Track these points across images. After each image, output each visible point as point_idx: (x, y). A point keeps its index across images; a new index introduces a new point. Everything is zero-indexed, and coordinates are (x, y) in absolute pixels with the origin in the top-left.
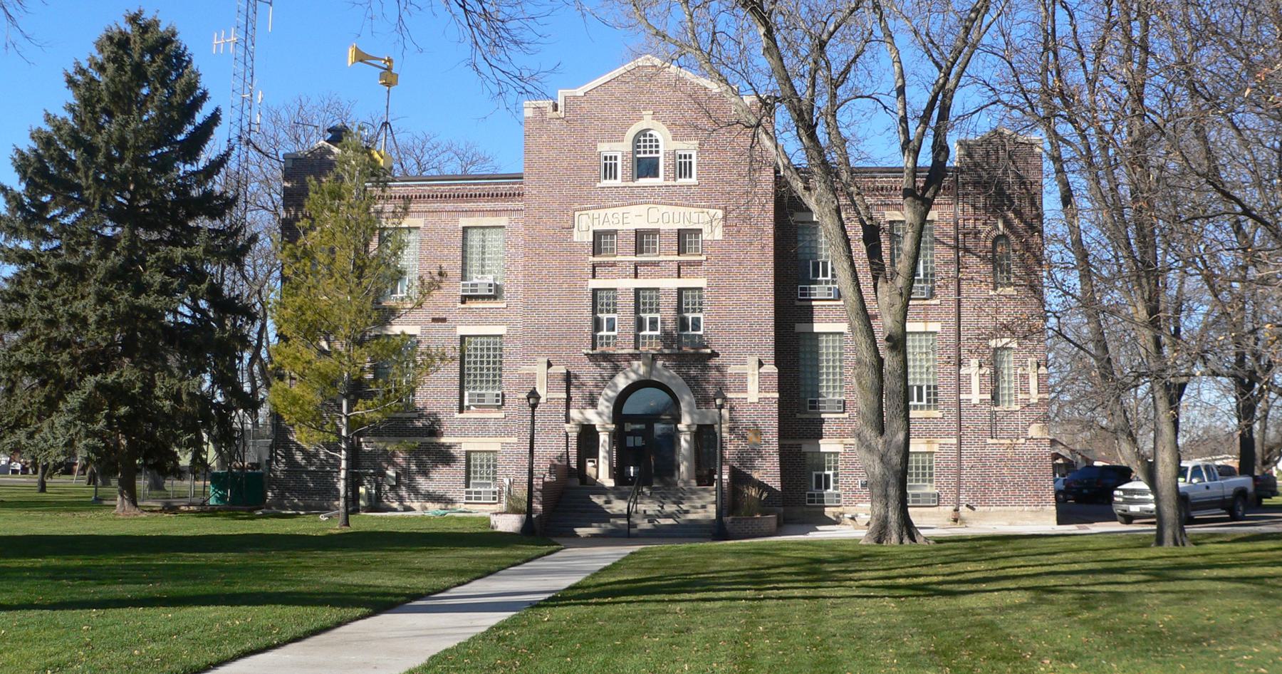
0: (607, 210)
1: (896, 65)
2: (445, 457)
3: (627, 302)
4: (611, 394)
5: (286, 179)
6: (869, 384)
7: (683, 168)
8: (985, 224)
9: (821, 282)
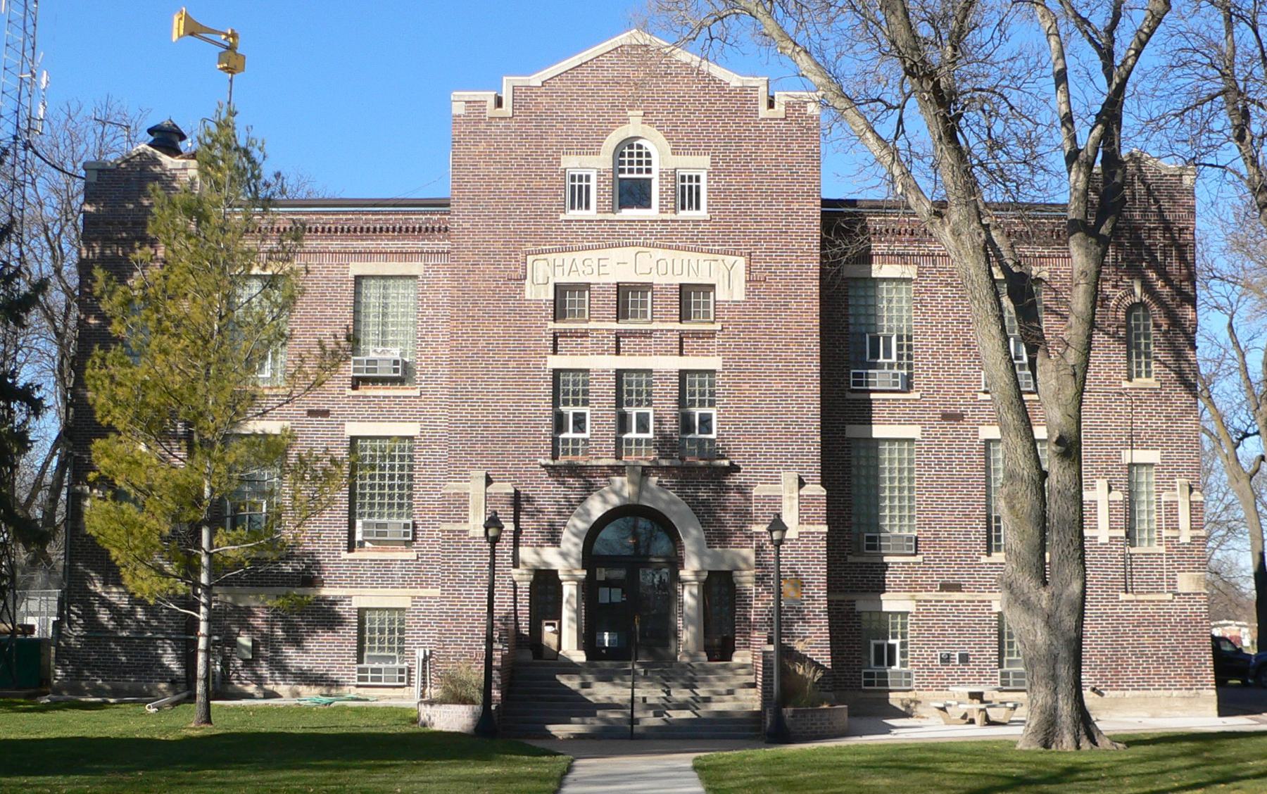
1: (1053, 40)
2: (327, 617)
3: (604, 390)
4: (583, 526)
5: (88, 200)
6: (1027, 508)
7: (687, 195)
8: (1115, 287)
9: (881, 366)
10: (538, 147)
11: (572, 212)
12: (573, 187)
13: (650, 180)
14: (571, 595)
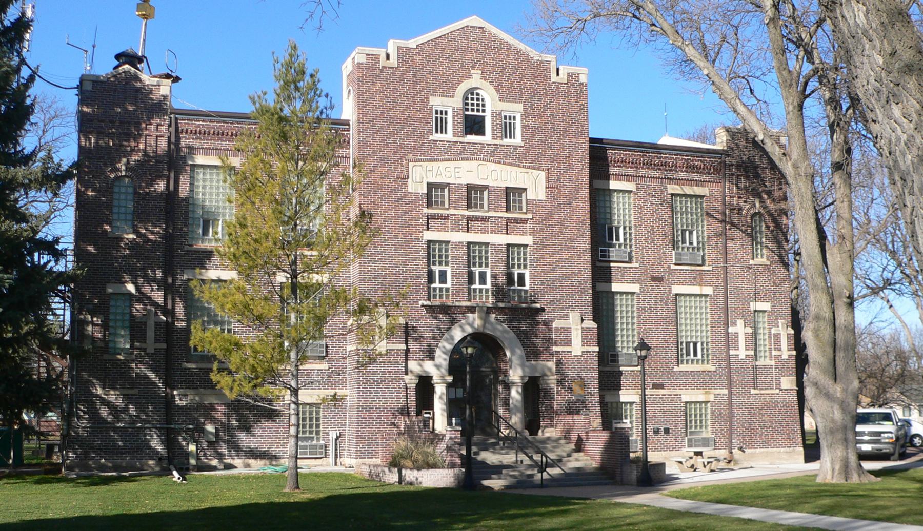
0: (440, 163)
4: (449, 347)
10: (415, 89)
11: (436, 135)
12: (437, 118)
13: (484, 117)
14: (442, 394)
